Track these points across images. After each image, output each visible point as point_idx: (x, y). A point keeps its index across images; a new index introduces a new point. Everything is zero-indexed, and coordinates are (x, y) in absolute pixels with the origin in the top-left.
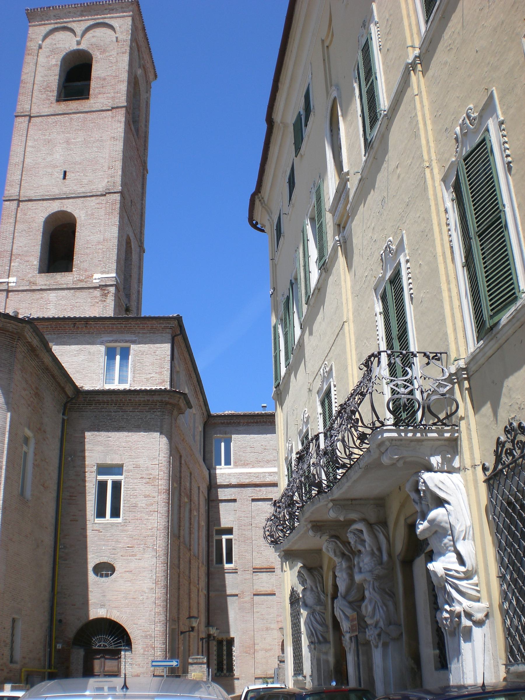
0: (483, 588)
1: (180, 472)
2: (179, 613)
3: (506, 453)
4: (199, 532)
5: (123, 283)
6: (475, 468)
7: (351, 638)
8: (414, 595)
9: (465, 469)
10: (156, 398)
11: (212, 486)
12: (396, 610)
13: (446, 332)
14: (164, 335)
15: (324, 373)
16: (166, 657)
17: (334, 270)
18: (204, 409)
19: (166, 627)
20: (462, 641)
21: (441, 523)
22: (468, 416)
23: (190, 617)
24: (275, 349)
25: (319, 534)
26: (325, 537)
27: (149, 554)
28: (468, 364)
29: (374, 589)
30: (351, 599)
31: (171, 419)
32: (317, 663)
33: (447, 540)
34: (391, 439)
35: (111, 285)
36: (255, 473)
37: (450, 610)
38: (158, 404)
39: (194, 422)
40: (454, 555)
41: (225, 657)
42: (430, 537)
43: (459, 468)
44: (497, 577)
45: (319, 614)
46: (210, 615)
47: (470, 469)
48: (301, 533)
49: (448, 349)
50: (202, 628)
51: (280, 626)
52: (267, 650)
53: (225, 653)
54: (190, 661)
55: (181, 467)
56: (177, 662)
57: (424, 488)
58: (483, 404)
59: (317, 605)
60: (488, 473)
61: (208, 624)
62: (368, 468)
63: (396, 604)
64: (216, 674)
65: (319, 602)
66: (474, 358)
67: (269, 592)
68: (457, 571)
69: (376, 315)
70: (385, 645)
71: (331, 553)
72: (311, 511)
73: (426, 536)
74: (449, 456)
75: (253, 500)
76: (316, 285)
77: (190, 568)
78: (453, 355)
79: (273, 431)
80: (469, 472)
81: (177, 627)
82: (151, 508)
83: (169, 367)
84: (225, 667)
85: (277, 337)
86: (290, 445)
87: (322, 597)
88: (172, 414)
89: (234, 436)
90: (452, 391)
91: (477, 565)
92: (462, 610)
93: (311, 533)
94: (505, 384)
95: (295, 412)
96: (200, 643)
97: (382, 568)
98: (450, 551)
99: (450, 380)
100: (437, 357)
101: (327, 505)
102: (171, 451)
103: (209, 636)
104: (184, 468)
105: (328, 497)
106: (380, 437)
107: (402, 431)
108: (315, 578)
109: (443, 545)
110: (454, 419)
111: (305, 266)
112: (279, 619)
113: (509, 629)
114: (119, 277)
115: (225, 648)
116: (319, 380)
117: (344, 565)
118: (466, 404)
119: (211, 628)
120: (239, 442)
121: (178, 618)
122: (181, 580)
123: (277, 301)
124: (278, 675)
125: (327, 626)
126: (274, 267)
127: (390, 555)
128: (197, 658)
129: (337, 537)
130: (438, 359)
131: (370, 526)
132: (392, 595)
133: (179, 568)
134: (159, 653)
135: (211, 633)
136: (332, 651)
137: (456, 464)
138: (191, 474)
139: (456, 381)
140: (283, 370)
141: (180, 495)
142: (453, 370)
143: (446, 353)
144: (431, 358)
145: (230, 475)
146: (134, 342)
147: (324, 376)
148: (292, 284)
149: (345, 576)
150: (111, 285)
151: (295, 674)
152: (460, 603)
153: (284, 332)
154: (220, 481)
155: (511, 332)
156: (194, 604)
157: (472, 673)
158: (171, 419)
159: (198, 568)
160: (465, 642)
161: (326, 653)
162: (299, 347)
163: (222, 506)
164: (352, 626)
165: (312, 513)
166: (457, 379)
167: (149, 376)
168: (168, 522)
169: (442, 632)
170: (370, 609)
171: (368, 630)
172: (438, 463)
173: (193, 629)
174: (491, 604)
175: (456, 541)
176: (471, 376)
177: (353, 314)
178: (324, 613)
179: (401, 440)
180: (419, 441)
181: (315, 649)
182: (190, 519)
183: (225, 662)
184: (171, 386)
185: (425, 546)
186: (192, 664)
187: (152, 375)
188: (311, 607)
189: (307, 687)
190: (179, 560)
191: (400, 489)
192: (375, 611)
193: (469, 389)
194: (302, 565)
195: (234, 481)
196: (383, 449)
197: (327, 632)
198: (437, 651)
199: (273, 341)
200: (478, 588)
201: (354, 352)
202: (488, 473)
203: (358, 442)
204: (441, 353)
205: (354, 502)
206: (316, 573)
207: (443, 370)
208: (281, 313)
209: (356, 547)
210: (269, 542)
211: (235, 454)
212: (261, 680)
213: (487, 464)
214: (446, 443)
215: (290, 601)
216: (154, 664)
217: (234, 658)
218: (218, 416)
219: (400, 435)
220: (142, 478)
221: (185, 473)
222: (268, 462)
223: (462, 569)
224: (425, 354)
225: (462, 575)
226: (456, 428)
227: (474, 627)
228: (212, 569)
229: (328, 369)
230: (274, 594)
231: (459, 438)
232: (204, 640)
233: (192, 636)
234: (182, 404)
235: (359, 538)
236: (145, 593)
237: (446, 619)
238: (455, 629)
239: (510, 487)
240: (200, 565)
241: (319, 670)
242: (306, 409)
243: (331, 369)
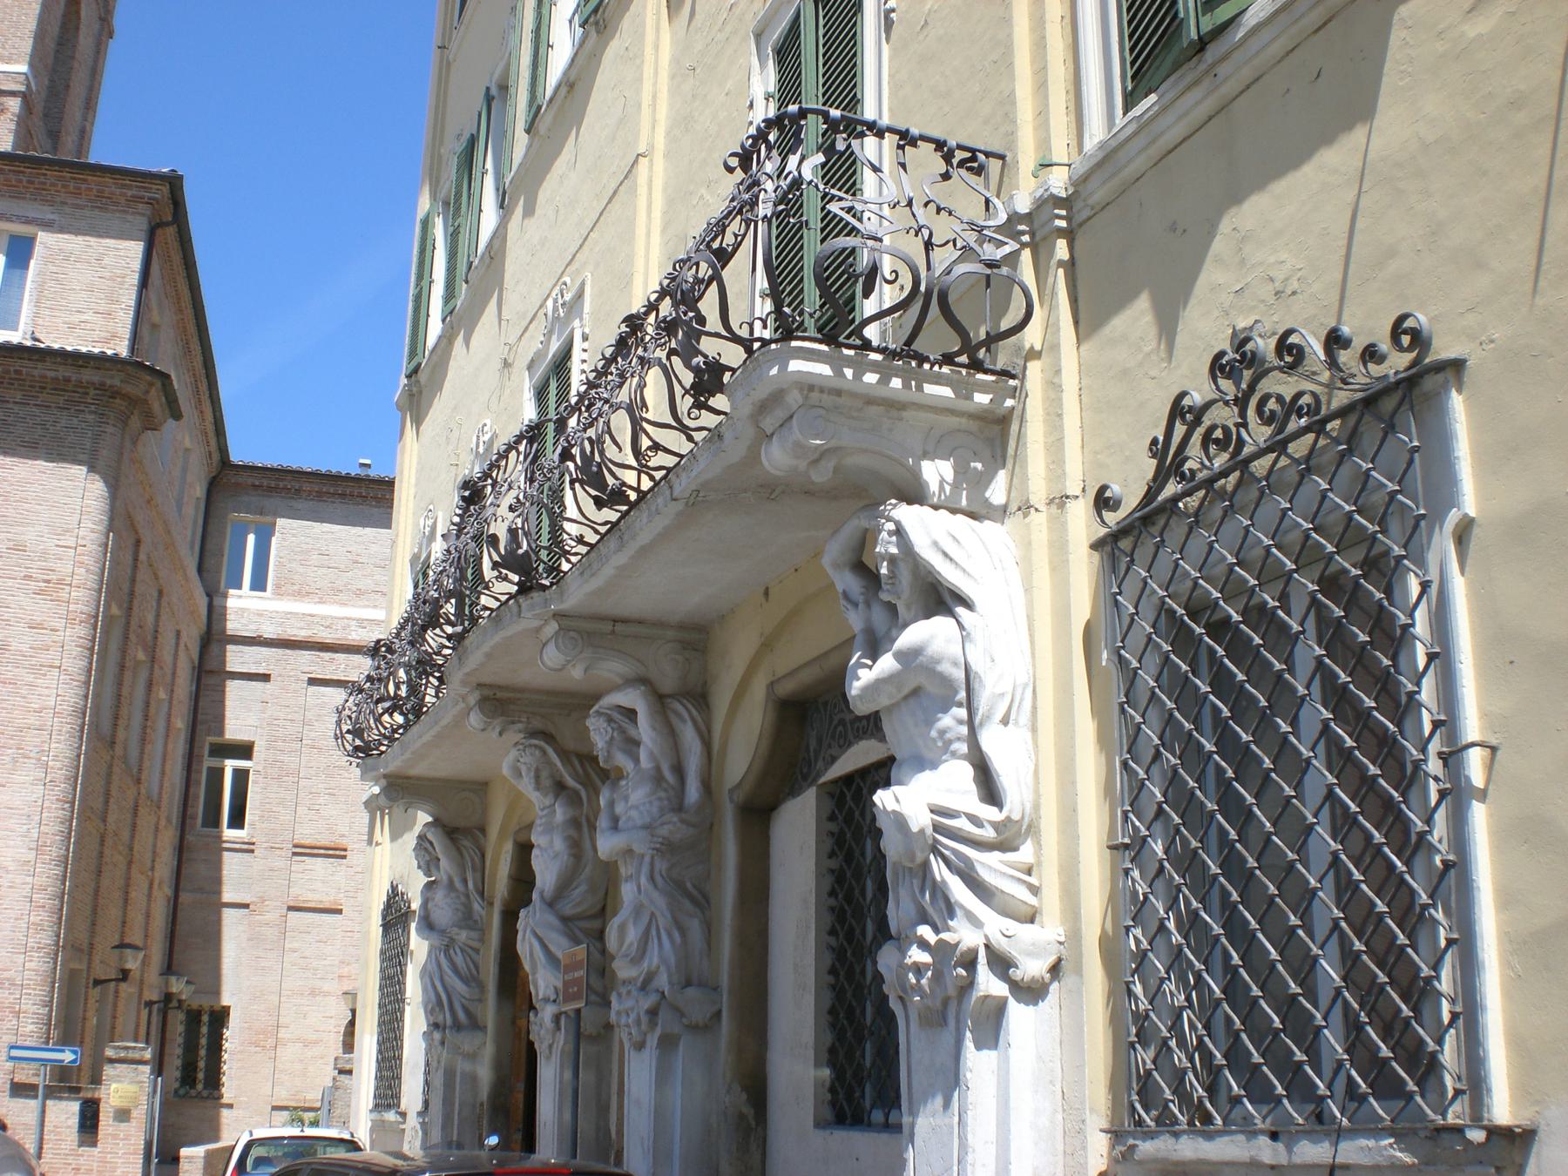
0: (1050, 879)
1: (133, 581)
2: (93, 933)
3: (1207, 440)
4: (166, 744)
5: (44, 95)
6: (1062, 506)
7: (557, 1018)
8: (767, 906)
9: (1026, 508)
10: (88, 375)
11: (214, 637)
12: (709, 945)
13: (1013, 92)
14: (130, 217)
15: (555, 309)
16: (48, 1038)
17: (626, 23)
18: (213, 442)
19: (55, 963)
20: (969, 1044)
21: (938, 662)
22: (1055, 348)
23: (122, 946)
24: (420, 277)
25: (497, 723)
26: (514, 735)
27: (27, 775)
28: (1079, 183)
29: (652, 878)
30: (568, 909)
31: (123, 438)
32: (445, 1082)
33: (951, 720)
34: (809, 386)
35: (13, 94)
36: (324, 617)
37: (941, 941)
38: (92, 392)
39: (185, 470)
40: (965, 771)
41: (203, 1052)
42: (890, 709)
43: (1004, 509)
44: (1110, 847)
46: (176, 948)
47: (1042, 507)
48: (444, 722)
49: (1011, 135)
50: (153, 975)
51: (345, 989)
52: (307, 1044)
53: (204, 1041)
54: (109, 1053)
55: (135, 567)
56: (75, 1052)
57: (894, 550)
58: (1122, 301)
59: (461, 928)
60: (1112, 518)
61: (169, 969)
62: (697, 503)
63: (709, 929)
64: (176, 1091)
65: (467, 919)
66: (1109, 156)
67: (327, 905)
68: (974, 820)
69: (751, 106)
70: (667, 1043)
71: (526, 779)
72: (486, 648)
73: (883, 701)
74: (979, 466)
75: (313, 682)
76: (566, 73)
77: (134, 826)
78: (1026, 159)
79: (387, 524)
80: (1039, 520)
81: (84, 966)
82: (45, 658)
83: (133, 303)
84: (201, 1075)
85: (429, 247)
86: (430, 522)
87: (476, 906)
88: (125, 423)
89: (281, 523)
90: (1012, 259)
91: (1037, 807)
92: (981, 942)
93: (475, 719)
94: (1225, 226)
95: (456, 434)
96: (145, 1013)
97: (682, 821)
98: (954, 755)
99: (1009, 228)
100: (973, 161)
101: (538, 630)
102: (111, 519)
103: (168, 997)
104: (143, 574)
105: (546, 603)
106: (774, 371)
107: (849, 362)
108: (461, 854)
109: (934, 734)
110: (1003, 357)
111: (537, 32)
112: (345, 971)
113: (1141, 1018)
114: (35, 77)
115: (204, 1030)
116: (539, 328)
117: (560, 814)
118: (1052, 308)
119: (173, 979)
120: (296, 538)
121: (91, 945)
122: (107, 852)
123: (440, 156)
124: (332, 1103)
125: (482, 987)
126: (445, 67)
127: (707, 786)
128: (127, 1048)
129: (548, 737)
130: (979, 171)
131: (660, 700)
132: (702, 900)
133: (104, 821)
134: (31, 1027)
135: (174, 990)
136: (489, 1051)
137: (997, 492)
138: (161, 593)
139: (1026, 238)
140: (435, 328)
141: (126, 638)
142: (1023, 205)
143: (1002, 157)
144: (955, 161)
145: (261, 615)
146: (48, 226)
147: (556, 319)
148: (489, 99)
149: (559, 844)
150: (13, 94)
151: (376, 1106)
152: (975, 922)
153: (451, 229)
154: (233, 626)
155: (1277, 48)
156: (136, 917)
157: (993, 1149)
158: (123, 438)
159: (157, 829)
160: (979, 1047)
161: (472, 1057)
162: (487, 260)
163: (233, 687)
164: (566, 984)
165: (488, 656)
166: (1032, 234)
167: (76, 318)
168: (86, 697)
169: (892, 1016)
170: (633, 935)
171: (620, 995)
172: (942, 481)
173: (125, 975)
174: (1074, 936)
175: (981, 724)
176: (1081, 225)
177: (668, 133)
178: (477, 951)
179: (838, 393)
180: (894, 406)
181: (443, 1043)
182: (147, 704)
183: (202, 1064)
184: (132, 349)
185: (820, 764)
186: (112, 1061)
187: (84, 317)
188: (443, 932)
189: (406, 1149)
190: (107, 802)
191: (767, 593)
192: (646, 943)
193: (1071, 266)
194: (430, 819)
195: (269, 632)
196: (769, 424)
197: (480, 1000)
198: (826, 1072)
199: (411, 305)
200: (1033, 880)
201: (656, 238)
202: (1112, 518)
203: (684, 404)
204: (987, 154)
205: (619, 628)
206: (466, 843)
207: (987, 201)
208: (447, 185)
209: (609, 757)
210: (349, 748)
211: (280, 565)
212: (285, 1114)
213: (1115, 489)
214: (973, 425)
215: (384, 918)
216: (15, 1053)
217: (225, 1057)
218: (246, 468)
219: (839, 373)
220: (28, 577)
221: (145, 588)
222: (359, 593)
223: (989, 813)
224: (940, 145)
225: (989, 833)
226: (1012, 382)
227: (1012, 1002)
228: (189, 838)
229: (568, 297)
230: (340, 912)
231: (1017, 413)
232: (156, 1007)
233: (122, 994)
234: (157, 404)
236: (8, 872)
237: (918, 969)
238: (946, 1002)
239: (1194, 560)
240: (163, 822)
241: (448, 1101)
242: (488, 422)
243: (580, 295)
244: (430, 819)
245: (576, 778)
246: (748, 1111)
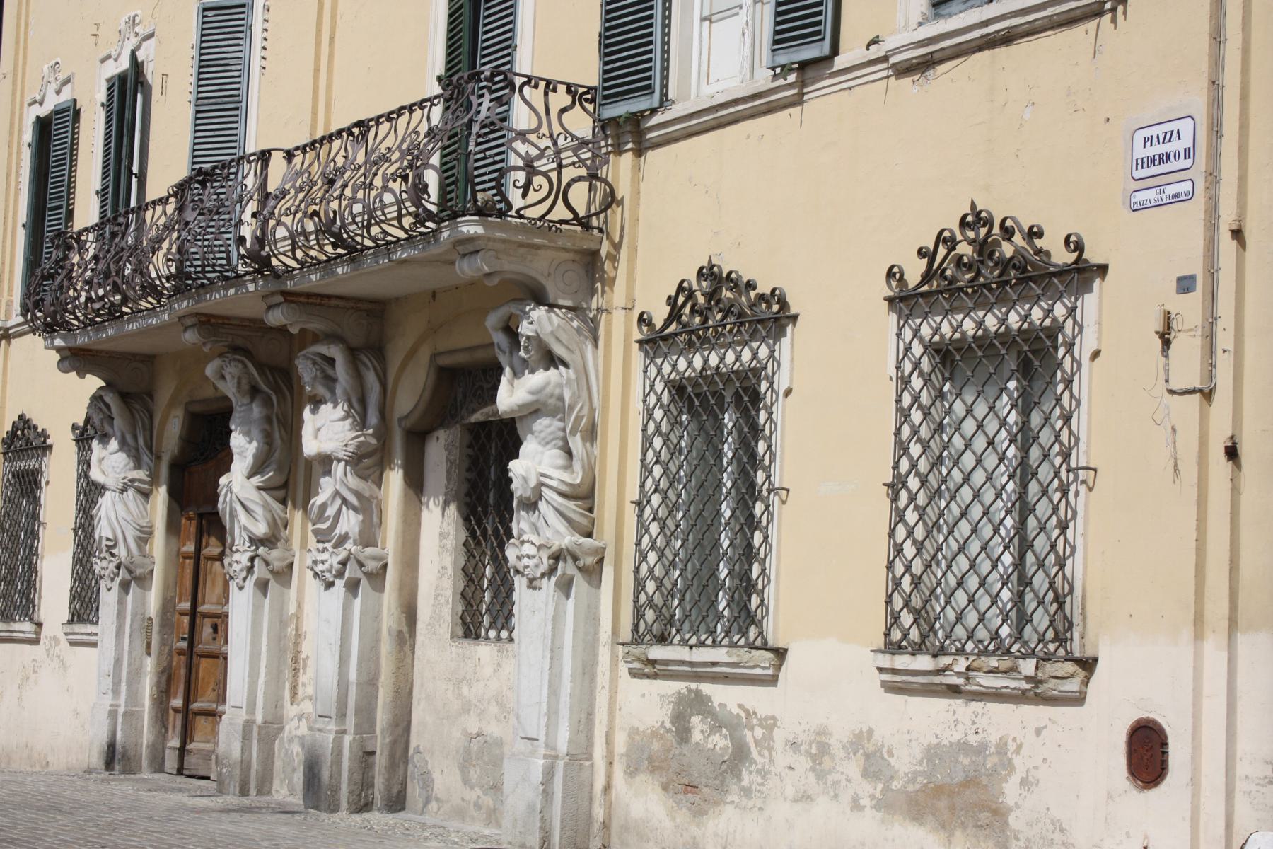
42: (521, 418)
131: (353, 354)
185: (464, 412)
194: (103, 384)
205: (325, 301)
206: (137, 406)
214: (577, 257)
244: (103, 384)
245: (268, 384)
246: (405, 629)
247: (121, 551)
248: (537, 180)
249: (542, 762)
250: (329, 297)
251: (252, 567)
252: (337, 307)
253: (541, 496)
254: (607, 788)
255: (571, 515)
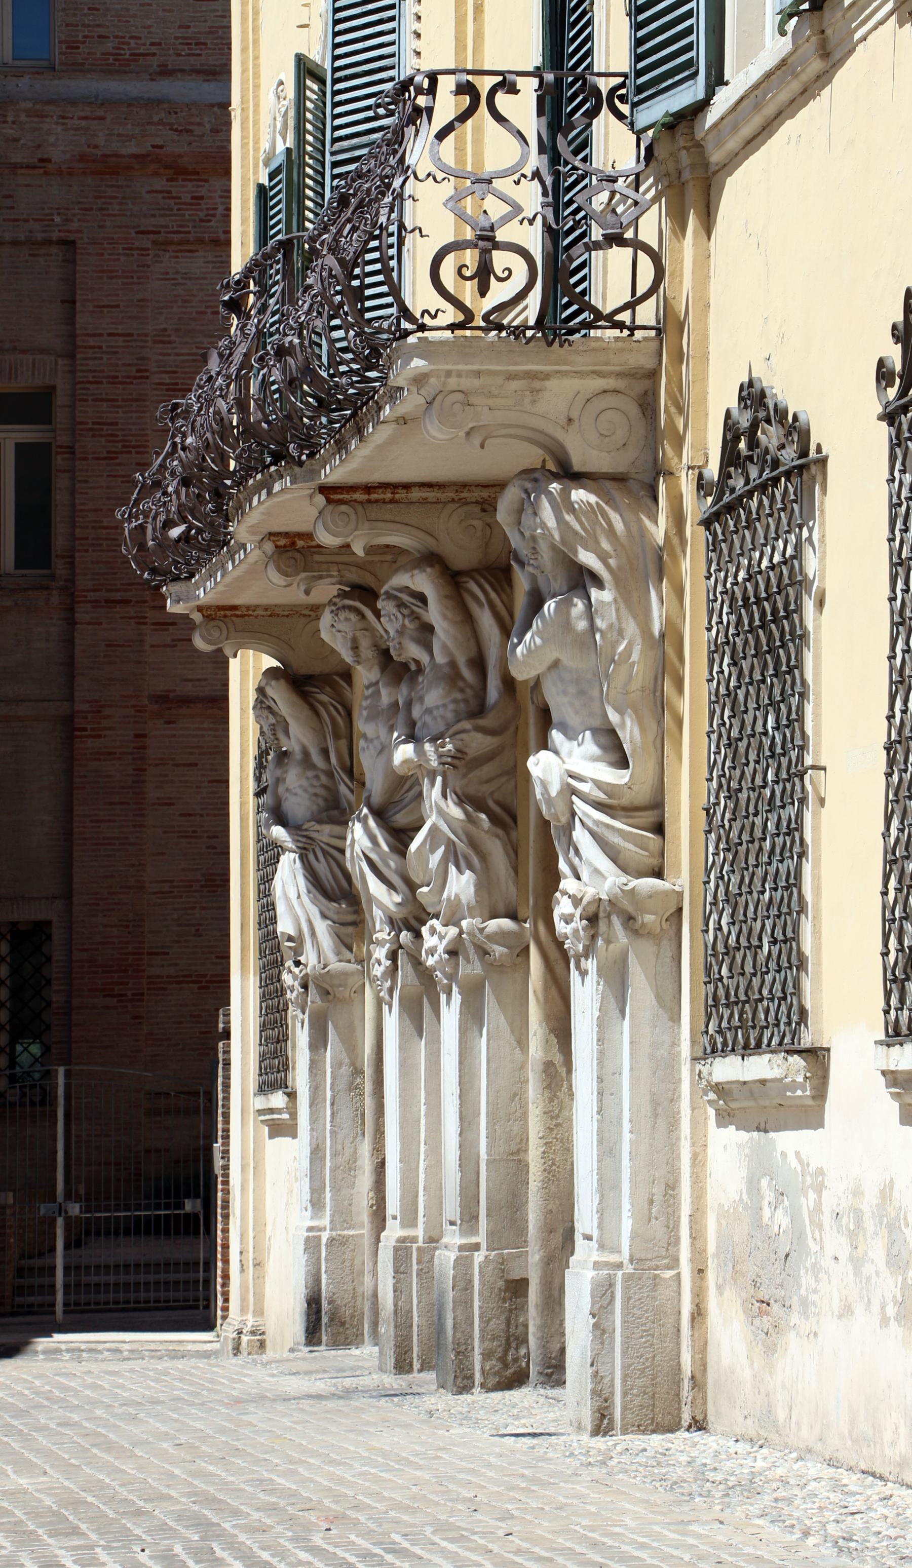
12: (516, 870)
45: (325, 853)
59: (320, 822)
87: (343, 789)
131: (453, 579)
205: (401, 495)
206: (324, 698)
235: (416, 617)
246: (558, 1058)
247: (310, 957)
248: (500, 260)
249: (590, 1274)
250: (407, 486)
251: (395, 967)
252: (425, 502)
253: (573, 814)
254: (699, 1314)
255: (616, 840)
